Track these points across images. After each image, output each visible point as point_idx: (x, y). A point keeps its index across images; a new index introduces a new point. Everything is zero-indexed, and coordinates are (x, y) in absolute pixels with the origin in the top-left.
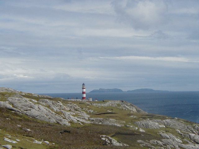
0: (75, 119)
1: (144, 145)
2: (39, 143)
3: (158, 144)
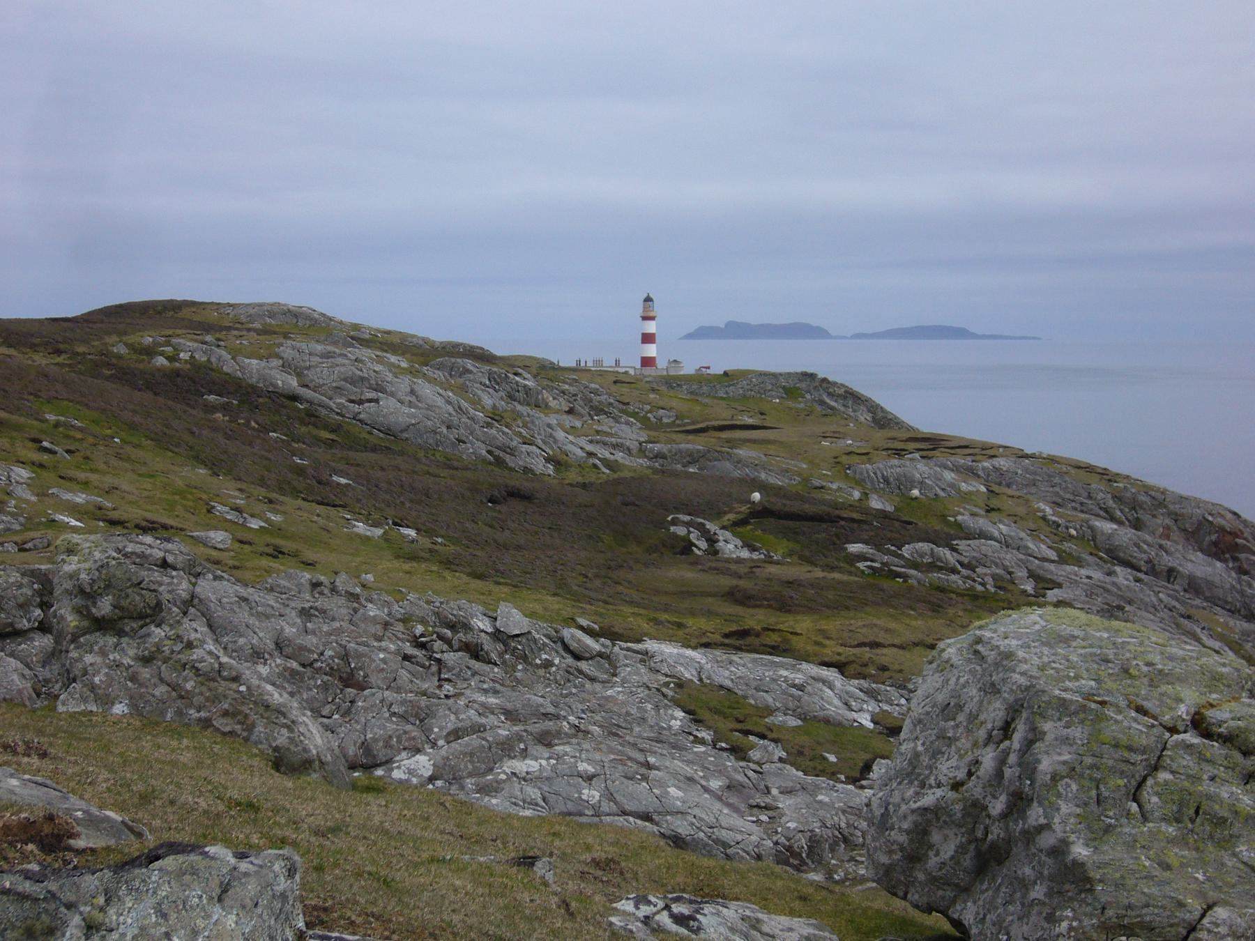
0: (576, 447)
1: (876, 565)
2: (369, 533)
3: (939, 564)
